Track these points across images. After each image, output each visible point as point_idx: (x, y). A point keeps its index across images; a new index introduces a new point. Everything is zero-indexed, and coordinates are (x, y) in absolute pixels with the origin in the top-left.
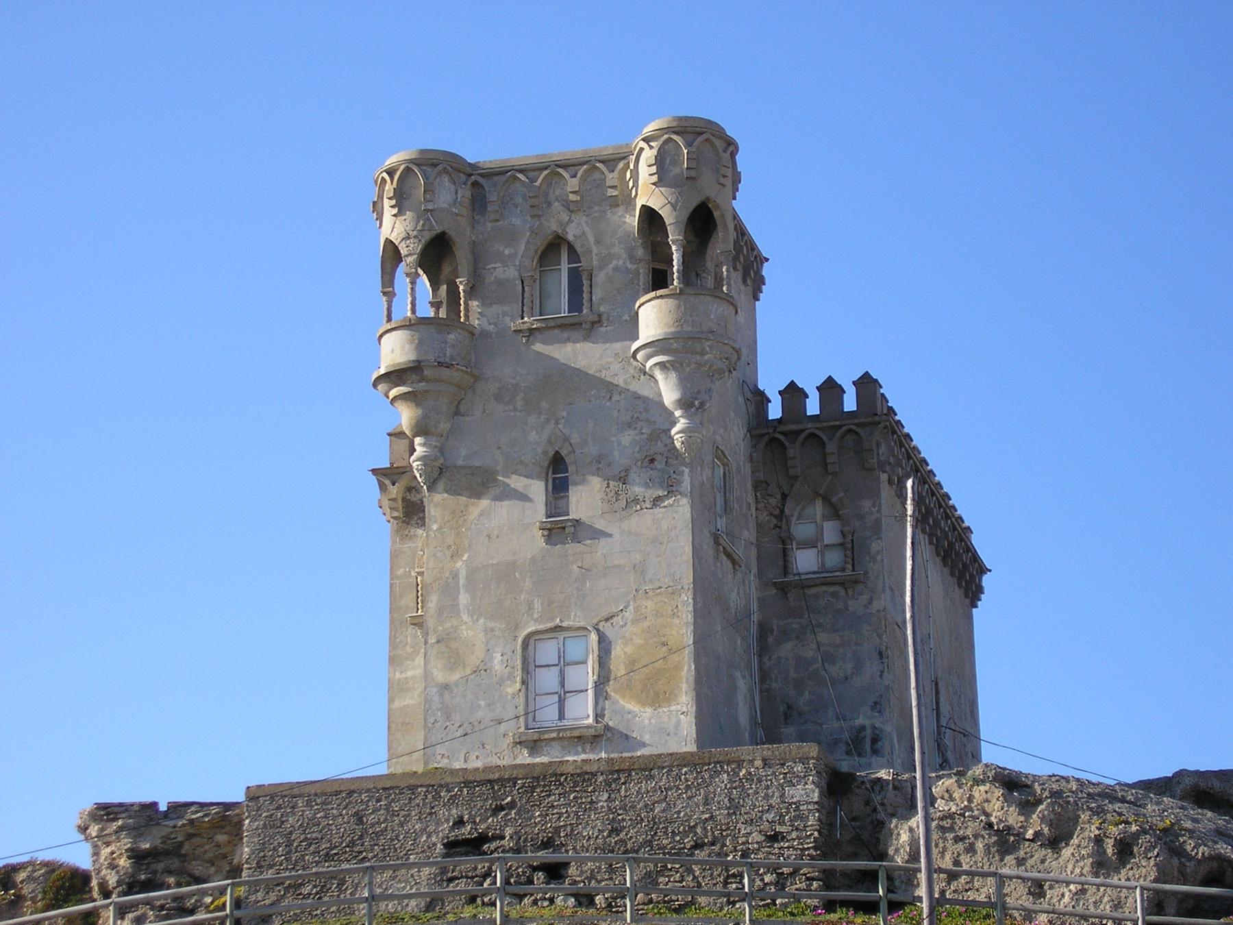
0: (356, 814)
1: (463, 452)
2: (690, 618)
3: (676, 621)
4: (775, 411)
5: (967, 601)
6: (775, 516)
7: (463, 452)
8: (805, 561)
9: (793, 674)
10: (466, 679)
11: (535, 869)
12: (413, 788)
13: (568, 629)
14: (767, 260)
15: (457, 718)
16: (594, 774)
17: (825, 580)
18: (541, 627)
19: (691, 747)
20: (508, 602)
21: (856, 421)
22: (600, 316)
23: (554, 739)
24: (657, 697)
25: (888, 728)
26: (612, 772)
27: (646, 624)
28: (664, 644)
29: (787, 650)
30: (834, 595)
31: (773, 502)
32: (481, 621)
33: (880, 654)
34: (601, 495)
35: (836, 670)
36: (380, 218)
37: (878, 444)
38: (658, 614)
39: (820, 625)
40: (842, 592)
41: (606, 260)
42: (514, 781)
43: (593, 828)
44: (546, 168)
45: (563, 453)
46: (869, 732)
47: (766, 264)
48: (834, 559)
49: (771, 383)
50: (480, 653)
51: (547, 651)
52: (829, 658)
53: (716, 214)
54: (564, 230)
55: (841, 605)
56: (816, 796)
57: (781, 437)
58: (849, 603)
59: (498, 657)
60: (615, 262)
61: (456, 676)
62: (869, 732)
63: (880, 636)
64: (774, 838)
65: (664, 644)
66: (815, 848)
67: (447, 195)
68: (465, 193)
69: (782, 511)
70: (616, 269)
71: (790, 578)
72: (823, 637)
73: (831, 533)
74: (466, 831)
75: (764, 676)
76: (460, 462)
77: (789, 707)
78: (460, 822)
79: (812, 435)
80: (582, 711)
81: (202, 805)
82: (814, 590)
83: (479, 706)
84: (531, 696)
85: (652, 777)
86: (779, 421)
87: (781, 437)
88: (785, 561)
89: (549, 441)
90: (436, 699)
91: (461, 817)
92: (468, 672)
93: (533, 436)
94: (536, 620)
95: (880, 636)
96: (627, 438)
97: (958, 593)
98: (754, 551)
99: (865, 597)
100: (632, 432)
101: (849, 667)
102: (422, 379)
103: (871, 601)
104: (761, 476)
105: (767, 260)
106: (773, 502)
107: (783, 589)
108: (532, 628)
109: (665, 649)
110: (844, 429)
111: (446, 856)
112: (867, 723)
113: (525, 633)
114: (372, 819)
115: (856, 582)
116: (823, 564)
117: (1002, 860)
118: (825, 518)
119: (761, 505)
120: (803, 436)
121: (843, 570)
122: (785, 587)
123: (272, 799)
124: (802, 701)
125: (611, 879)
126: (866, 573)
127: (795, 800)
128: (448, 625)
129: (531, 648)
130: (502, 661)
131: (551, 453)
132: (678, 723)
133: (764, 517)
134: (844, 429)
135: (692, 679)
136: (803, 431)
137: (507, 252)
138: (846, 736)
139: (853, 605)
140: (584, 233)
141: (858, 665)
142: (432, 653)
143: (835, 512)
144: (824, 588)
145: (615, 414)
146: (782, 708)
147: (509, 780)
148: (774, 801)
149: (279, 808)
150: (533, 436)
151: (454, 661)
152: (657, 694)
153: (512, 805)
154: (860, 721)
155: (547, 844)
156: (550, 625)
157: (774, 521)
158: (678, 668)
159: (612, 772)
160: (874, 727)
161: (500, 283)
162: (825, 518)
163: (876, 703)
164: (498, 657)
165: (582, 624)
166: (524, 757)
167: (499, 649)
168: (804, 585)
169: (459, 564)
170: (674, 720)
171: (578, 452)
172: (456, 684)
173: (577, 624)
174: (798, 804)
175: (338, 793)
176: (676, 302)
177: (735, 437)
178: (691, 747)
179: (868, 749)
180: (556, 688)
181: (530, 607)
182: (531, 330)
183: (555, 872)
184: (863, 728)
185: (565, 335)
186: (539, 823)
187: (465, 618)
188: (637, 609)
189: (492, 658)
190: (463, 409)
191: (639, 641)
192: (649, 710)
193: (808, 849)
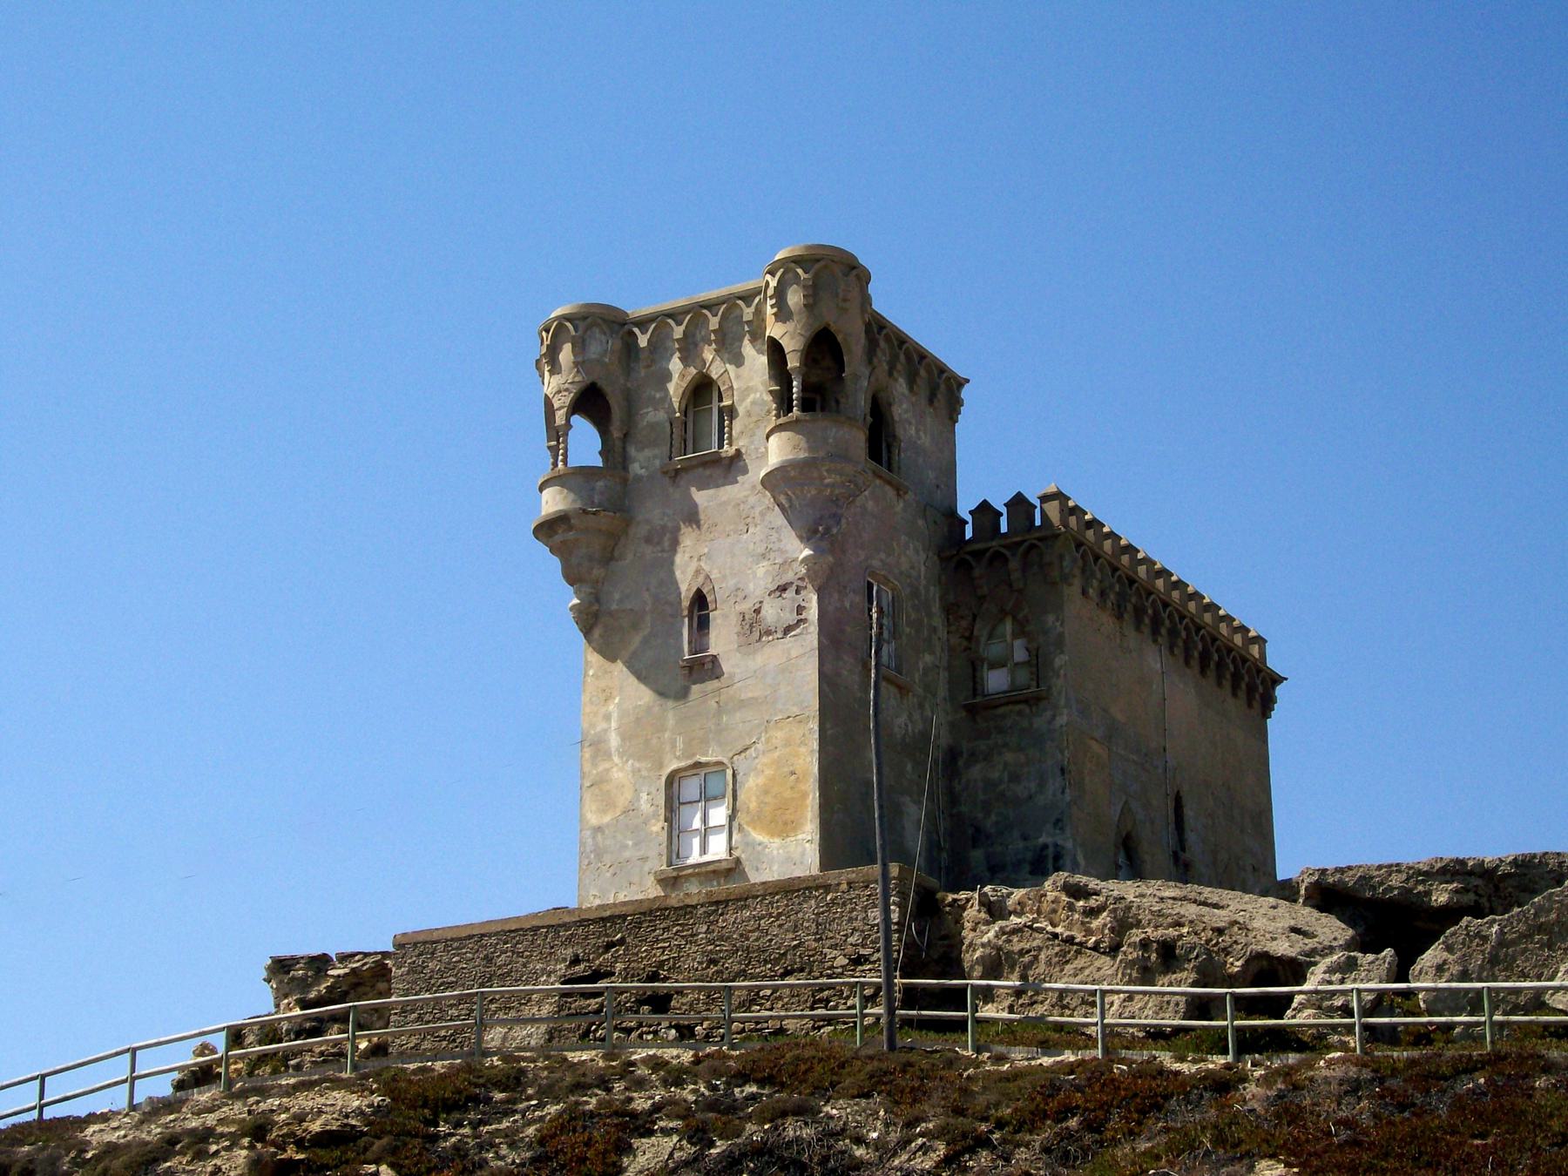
0: (486, 957)
1: (617, 596)
2: (816, 746)
3: (803, 749)
7: (617, 596)
8: (996, 681)
9: (981, 797)
10: (617, 819)
12: (535, 929)
13: (707, 764)
15: (607, 859)
16: (694, 907)
17: (1013, 698)
18: (682, 764)
19: (815, 871)
20: (654, 741)
23: (690, 875)
24: (784, 826)
25: (1069, 845)
26: (711, 904)
27: (777, 754)
28: (793, 773)
29: (976, 772)
30: (1020, 713)
31: (964, 623)
33: (1063, 770)
34: (738, 628)
35: (1020, 790)
36: (542, 376)
37: (1061, 557)
38: (788, 743)
39: (1005, 745)
40: (1027, 710)
41: (748, 391)
42: (624, 917)
43: (693, 958)
44: (688, 312)
46: (1051, 850)
48: (1023, 676)
49: (965, 507)
50: (628, 795)
51: (691, 789)
52: (1015, 778)
53: (840, 338)
55: (1025, 724)
59: (644, 796)
61: (607, 819)
62: (1051, 850)
63: (1062, 752)
64: (858, 961)
65: (793, 773)
67: (602, 346)
68: (614, 344)
70: (753, 403)
71: (979, 699)
72: (1009, 757)
73: (1020, 655)
75: (954, 799)
76: (614, 607)
77: (978, 830)
78: (576, 961)
81: (366, 955)
82: (1001, 710)
83: (626, 846)
84: (675, 833)
85: (746, 907)
88: (975, 683)
90: (590, 841)
91: (577, 956)
94: (678, 758)
95: (1062, 752)
96: (762, 569)
97: (1235, 706)
98: (944, 675)
99: (1049, 714)
100: (765, 563)
101: (1033, 786)
102: (571, 528)
103: (1054, 717)
104: (951, 598)
106: (964, 623)
107: (972, 710)
108: (675, 765)
112: (1049, 840)
113: (669, 770)
114: (499, 962)
118: (1015, 636)
119: (953, 628)
122: (977, 708)
123: (413, 946)
124: (989, 823)
126: (1050, 688)
128: (600, 769)
129: (676, 785)
130: (651, 801)
132: (803, 854)
133: (955, 640)
135: (817, 807)
136: (987, 549)
138: (1029, 855)
139: (1039, 723)
141: (1042, 784)
142: (587, 796)
143: (1020, 632)
145: (751, 546)
146: (970, 831)
147: (619, 917)
149: (420, 955)
151: (607, 803)
152: (785, 823)
153: (622, 942)
154: (1041, 840)
156: (690, 762)
157: (965, 643)
158: (804, 795)
159: (711, 904)
160: (1056, 845)
161: (653, 426)
162: (1015, 636)
163: (1058, 820)
164: (644, 796)
165: (720, 758)
167: (645, 789)
168: (993, 704)
169: (611, 707)
170: (800, 849)
172: (608, 825)
173: (714, 759)
175: (470, 937)
177: (912, 559)
178: (815, 871)
179: (1050, 866)
181: (674, 746)
182: (677, 471)
183: (660, 1003)
184: (1045, 846)
185: (708, 472)
186: (647, 954)
187: (616, 759)
188: (768, 741)
189: (638, 799)
190: (616, 554)
191: (768, 772)
192: (777, 840)
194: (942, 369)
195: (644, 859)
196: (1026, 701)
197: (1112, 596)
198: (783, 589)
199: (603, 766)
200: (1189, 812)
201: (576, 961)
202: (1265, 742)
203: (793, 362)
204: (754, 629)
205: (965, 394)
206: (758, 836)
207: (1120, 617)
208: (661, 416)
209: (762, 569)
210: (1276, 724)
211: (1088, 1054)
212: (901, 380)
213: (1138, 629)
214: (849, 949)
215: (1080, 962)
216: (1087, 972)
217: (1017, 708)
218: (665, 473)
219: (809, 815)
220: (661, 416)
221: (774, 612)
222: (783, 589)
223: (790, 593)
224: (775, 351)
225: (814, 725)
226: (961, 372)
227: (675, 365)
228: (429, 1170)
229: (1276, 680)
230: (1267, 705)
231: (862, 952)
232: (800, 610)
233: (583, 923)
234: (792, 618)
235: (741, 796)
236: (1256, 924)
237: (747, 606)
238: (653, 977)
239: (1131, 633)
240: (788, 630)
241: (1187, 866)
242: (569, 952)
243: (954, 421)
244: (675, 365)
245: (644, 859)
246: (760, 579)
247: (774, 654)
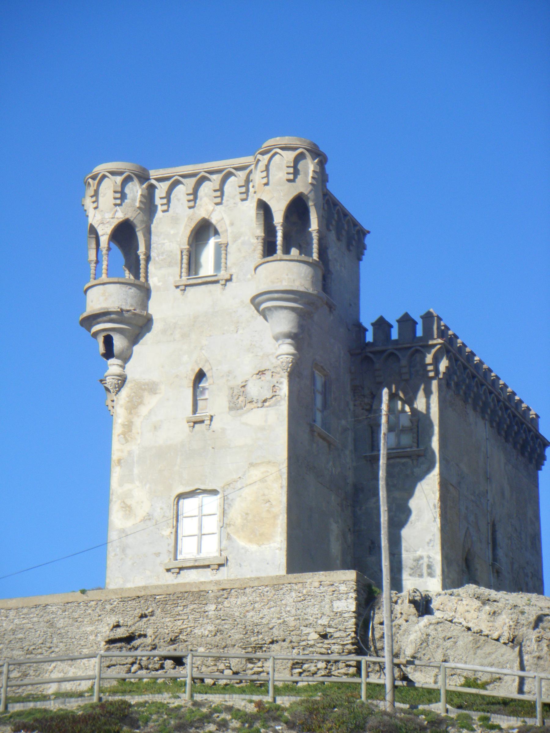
4: (369, 337)
5: (531, 466)
6: (367, 410)
11: (166, 658)
14: (369, 232)
21: (421, 344)
22: (231, 275)
24: (260, 537)
31: (366, 400)
32: (148, 486)
45: (205, 370)
46: (425, 561)
47: (368, 236)
49: (367, 319)
54: (210, 216)
56: (353, 608)
57: (371, 355)
58: (415, 470)
60: (242, 238)
62: (425, 561)
66: (353, 644)
69: (371, 406)
74: (121, 633)
78: (118, 626)
79: (392, 354)
80: (210, 550)
86: (396, 341)
87: (371, 355)
89: (196, 362)
92: (138, 520)
93: (185, 358)
105: (369, 232)
109: (268, 504)
110: (413, 349)
111: (108, 649)
112: (425, 554)
115: (419, 456)
116: (399, 443)
117: (475, 654)
120: (385, 354)
121: (411, 447)
125: (215, 665)
127: (339, 610)
131: (197, 370)
134: (413, 349)
137: (172, 232)
140: (223, 219)
144: (398, 460)
148: (327, 610)
150: (185, 358)
154: (419, 553)
155: (173, 641)
158: (275, 517)
160: (429, 557)
166: (170, 579)
171: (214, 369)
174: (341, 613)
176: (138, 291)
180: (196, 532)
184: (421, 558)
193: (347, 644)
194: (355, 224)
195: (158, 554)
196: (409, 457)
197: (464, 387)
198: (261, 373)
199: (127, 486)
200: (499, 536)
201: (118, 626)
202: (537, 486)
203: (278, 219)
204: (240, 400)
205: (368, 240)
206: (242, 543)
207: (465, 401)
210: (543, 475)
211: (530, 722)
212: (333, 232)
213: (475, 409)
214: (320, 629)
215: (488, 649)
216: (494, 656)
217: (404, 460)
218: (177, 287)
219: (279, 530)
221: (256, 389)
222: (261, 373)
224: (264, 209)
226: (366, 227)
229: (545, 444)
230: (538, 461)
231: (329, 630)
238: (173, 641)
239: (471, 412)
241: (498, 572)
242: (112, 620)
243: (360, 259)
245: (158, 554)
246: (246, 367)
247: (255, 417)
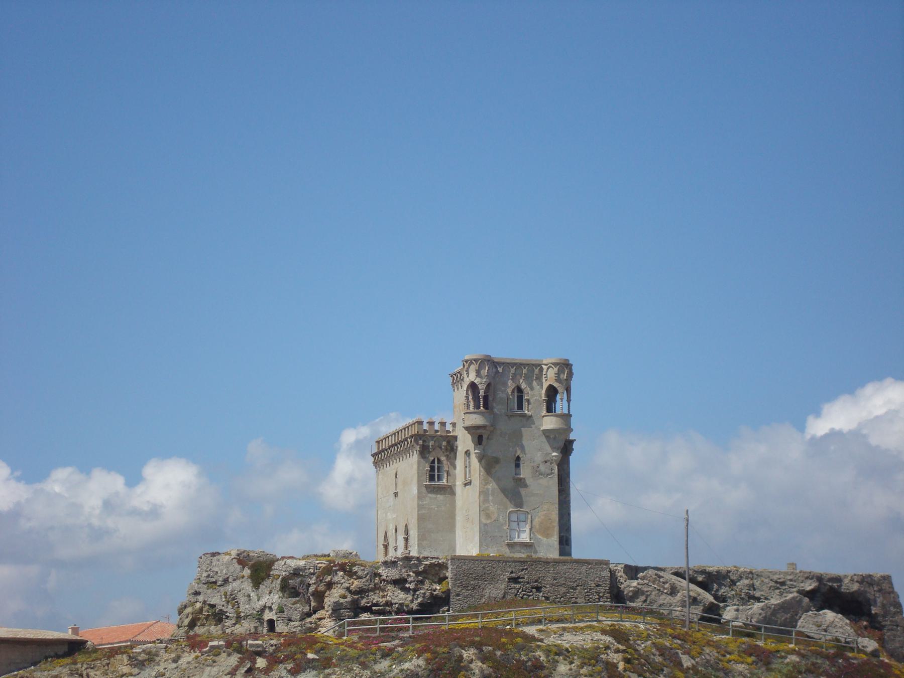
61: (489, 522)
78: (512, 572)
96: (539, 454)
158: (554, 527)
183: (538, 589)
201: (512, 572)
204: (537, 473)
208: (504, 396)
209: (539, 454)
220: (504, 396)
221: (543, 468)
223: (548, 464)
225: (557, 506)
227: (510, 383)
228: (123, 676)
232: (552, 470)
233: (514, 561)
234: (549, 472)
235: (534, 523)
236: (674, 614)
237: (535, 464)
240: (548, 475)
242: (510, 570)
244: (510, 383)
246: (539, 457)
